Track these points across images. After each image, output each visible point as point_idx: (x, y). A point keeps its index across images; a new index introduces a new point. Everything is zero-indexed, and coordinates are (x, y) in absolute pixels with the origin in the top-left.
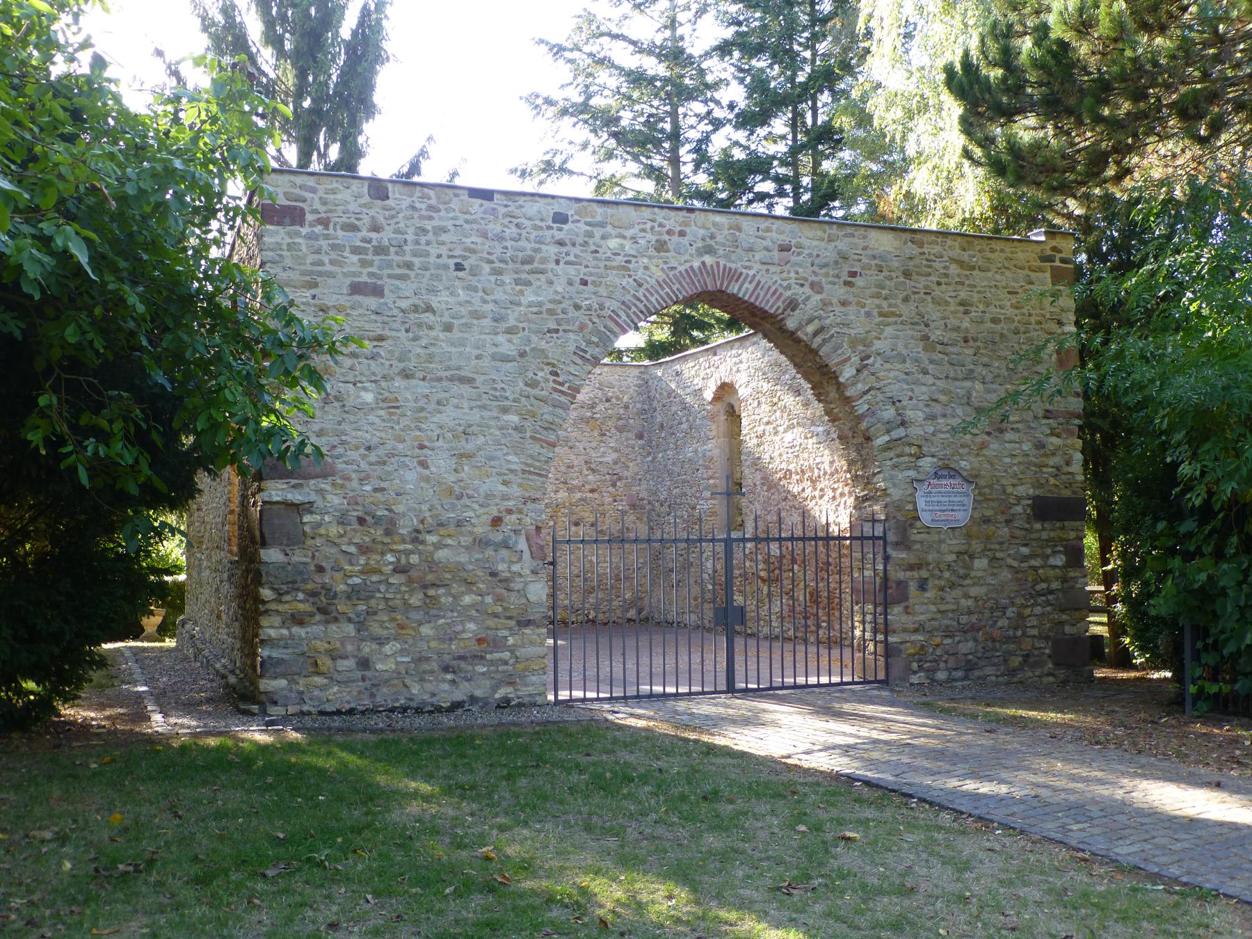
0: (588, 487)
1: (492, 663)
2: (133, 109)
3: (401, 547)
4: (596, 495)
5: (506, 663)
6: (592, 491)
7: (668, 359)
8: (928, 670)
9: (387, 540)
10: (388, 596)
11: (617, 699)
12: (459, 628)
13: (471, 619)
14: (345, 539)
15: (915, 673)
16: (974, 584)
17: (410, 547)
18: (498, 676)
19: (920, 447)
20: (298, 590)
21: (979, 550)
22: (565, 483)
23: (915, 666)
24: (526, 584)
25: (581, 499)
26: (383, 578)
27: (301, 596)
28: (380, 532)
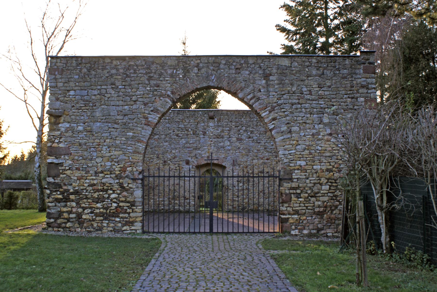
0: (266, 158)
1: (122, 218)
2: (180, 55)
3: (91, 178)
4: (269, 161)
5: (127, 218)
6: (267, 159)
7: (47, 101)
8: (299, 229)
9: (86, 175)
10: (86, 194)
11: (156, 232)
12: (110, 205)
13: (115, 202)
14: (73, 175)
15: (293, 230)
16: (322, 196)
17: (94, 178)
18: (124, 222)
19: (298, 141)
20: (58, 191)
21: (325, 182)
22: (256, 156)
23: (293, 227)
24: (134, 191)
25: (263, 162)
26: (85, 188)
27: (59, 193)
28: (84, 172)
